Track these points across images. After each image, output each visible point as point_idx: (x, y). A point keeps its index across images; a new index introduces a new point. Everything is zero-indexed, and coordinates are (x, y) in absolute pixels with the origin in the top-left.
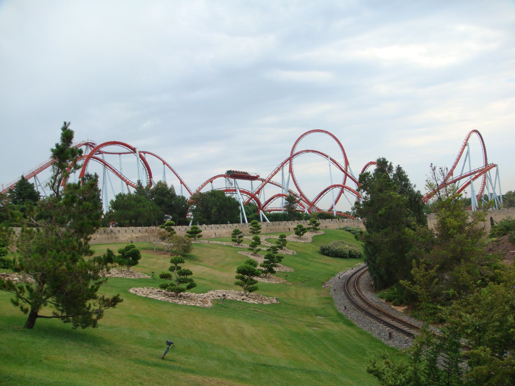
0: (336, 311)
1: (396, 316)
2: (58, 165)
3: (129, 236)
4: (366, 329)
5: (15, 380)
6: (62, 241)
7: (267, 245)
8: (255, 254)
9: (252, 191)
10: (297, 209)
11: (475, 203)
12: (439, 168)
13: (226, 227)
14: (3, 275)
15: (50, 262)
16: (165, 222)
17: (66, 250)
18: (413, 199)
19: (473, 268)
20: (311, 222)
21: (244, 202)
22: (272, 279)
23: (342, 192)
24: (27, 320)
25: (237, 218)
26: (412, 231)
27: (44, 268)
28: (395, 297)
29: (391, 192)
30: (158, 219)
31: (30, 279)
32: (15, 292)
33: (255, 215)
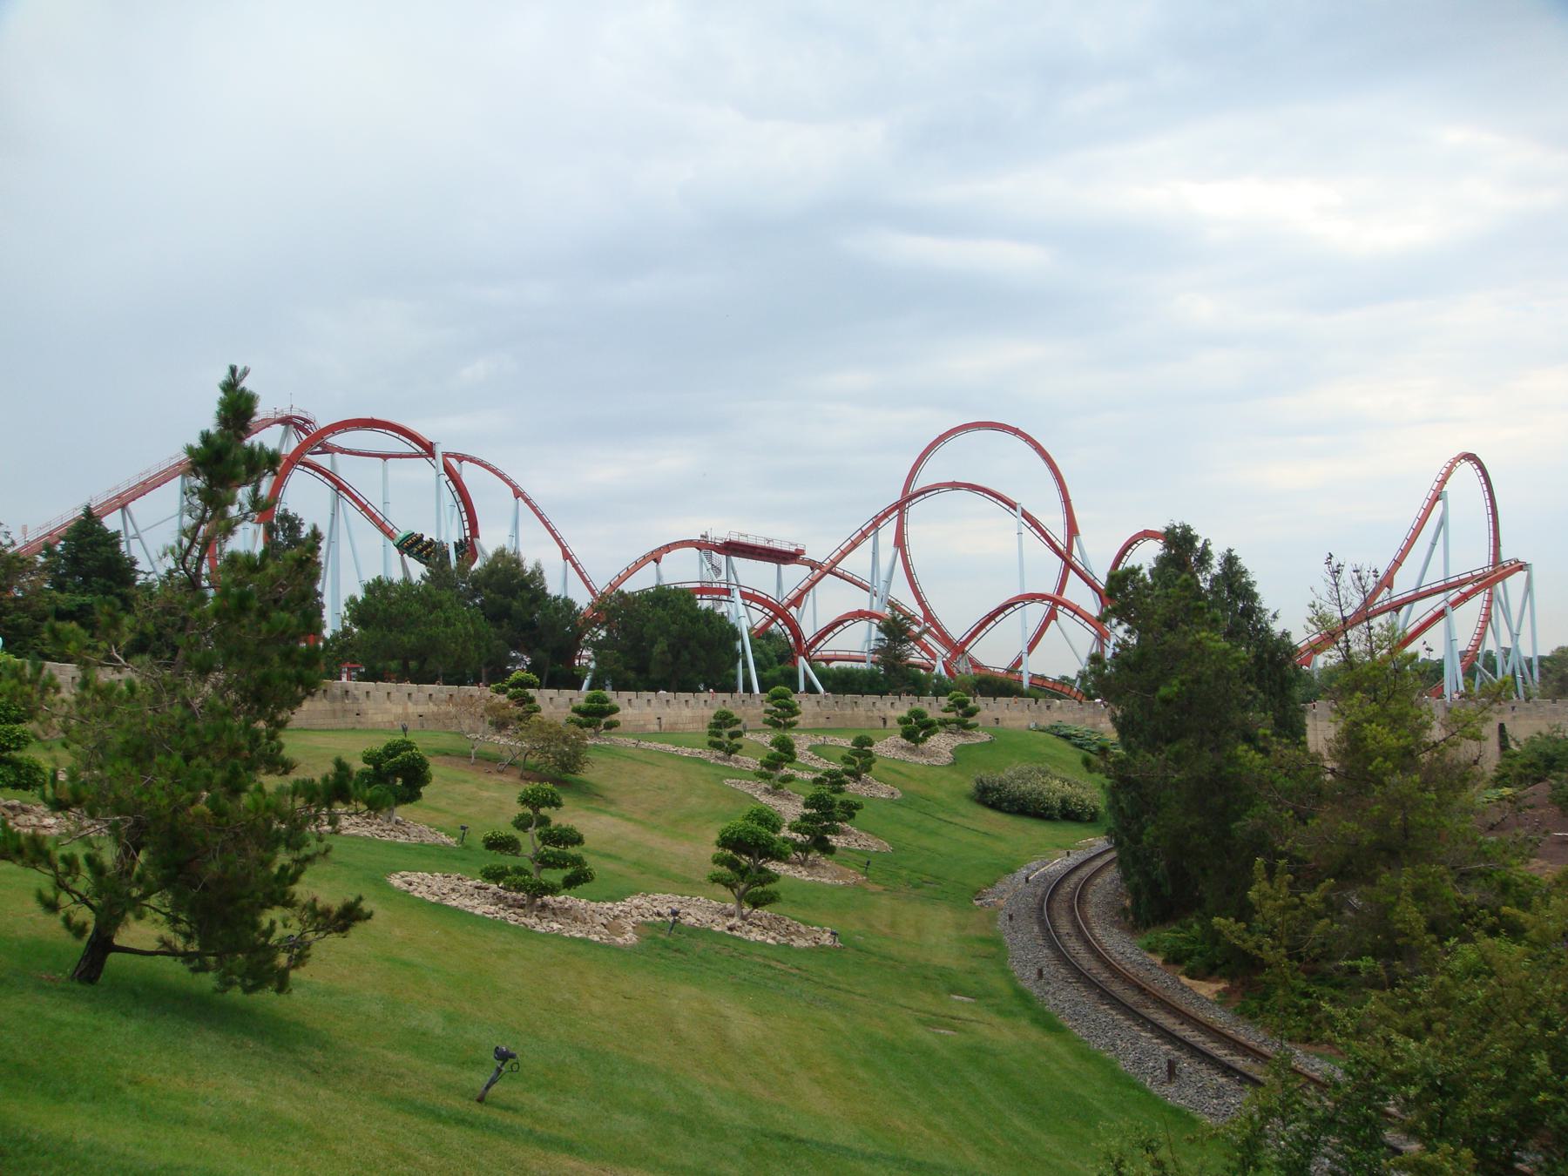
0: (1012, 981)
1: (1192, 1010)
2: (203, 496)
3: (399, 710)
4: (1098, 1045)
5: (45, 1153)
6: (199, 725)
7: (812, 763)
8: (775, 791)
9: (778, 597)
10: (911, 659)
11: (1453, 678)
12: (1351, 569)
13: (692, 701)
14: (12, 808)
15: (163, 788)
16: (510, 673)
17: (212, 754)
18: (1266, 656)
19: (1438, 880)
20: (951, 703)
21: (753, 628)
22: (822, 871)
23: (1052, 615)
24: (79, 958)
25: (727, 676)
26: (1257, 756)
27: (142, 804)
28: (1193, 950)
29: (1203, 631)
30: (488, 665)
31: (97, 831)
32: (50, 872)
33: (782, 671)
